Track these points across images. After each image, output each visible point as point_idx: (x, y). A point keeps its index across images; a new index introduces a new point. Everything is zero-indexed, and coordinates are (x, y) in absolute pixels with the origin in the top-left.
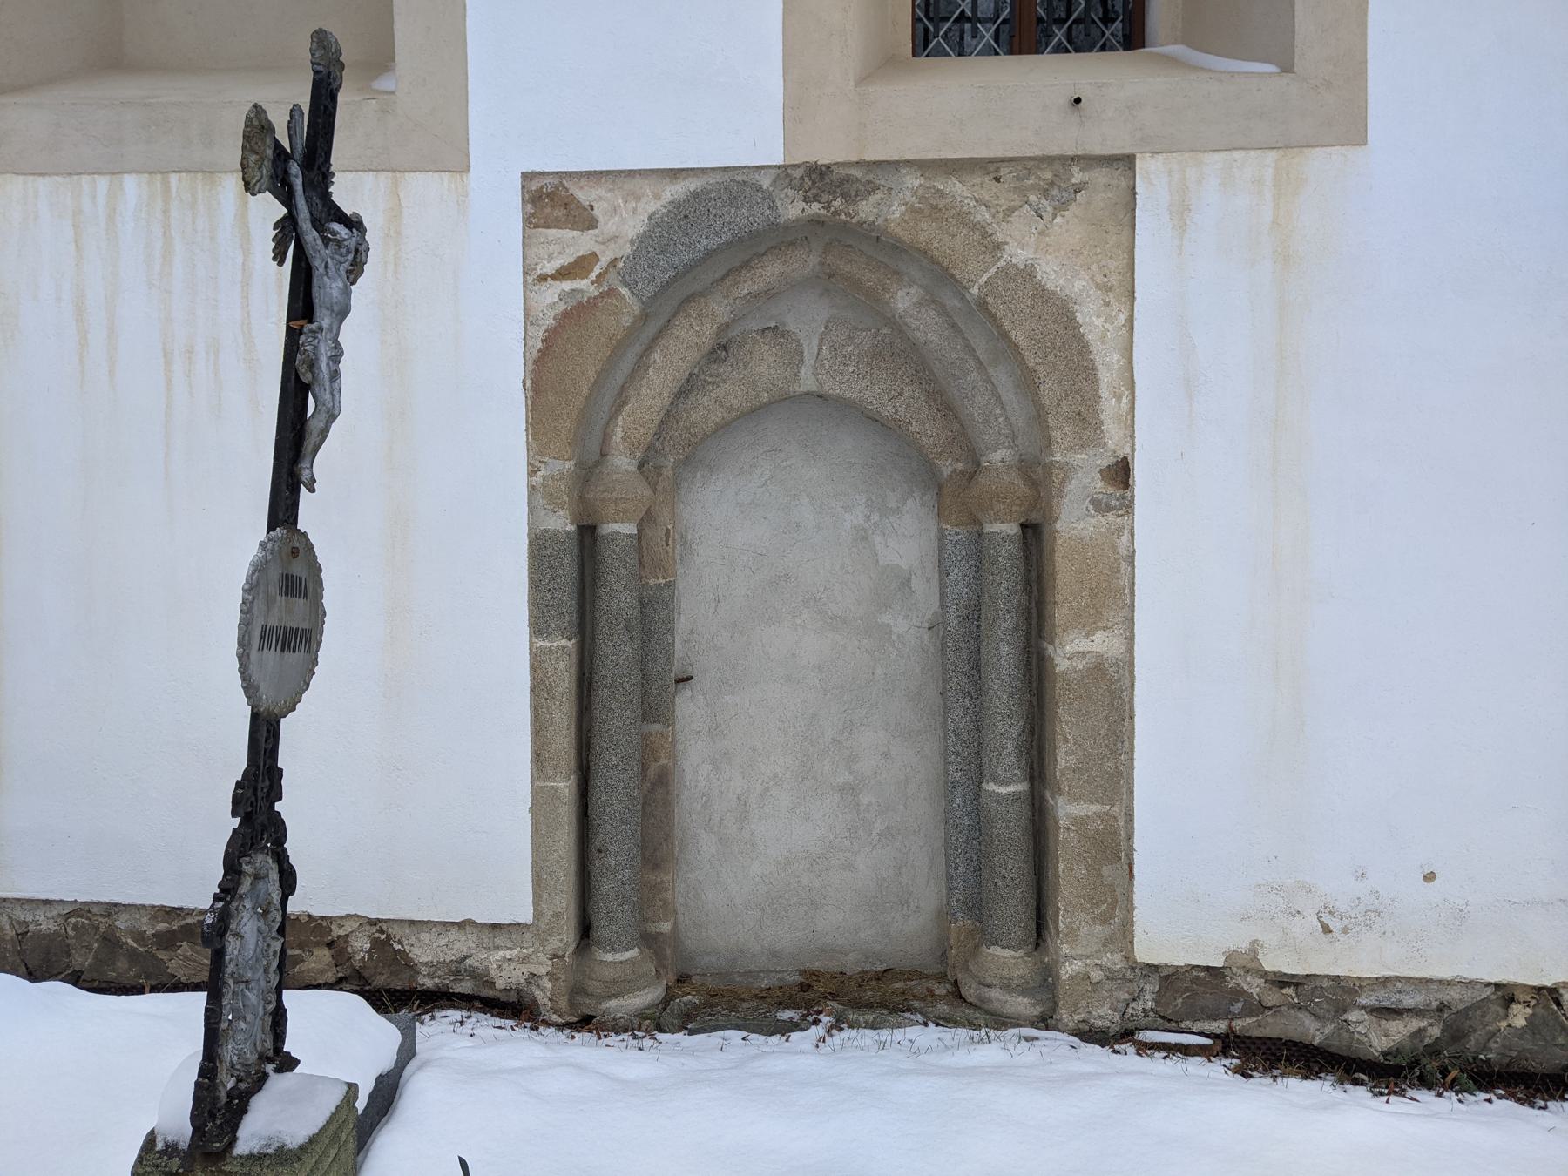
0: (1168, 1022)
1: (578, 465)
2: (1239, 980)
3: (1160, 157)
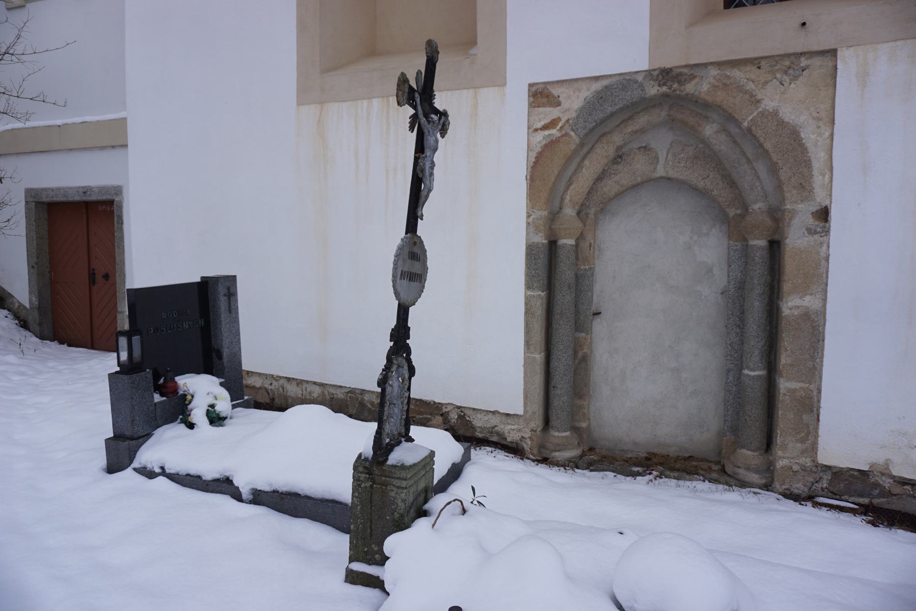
0: (834, 495)
1: (551, 213)
2: (877, 478)
3: (852, 49)
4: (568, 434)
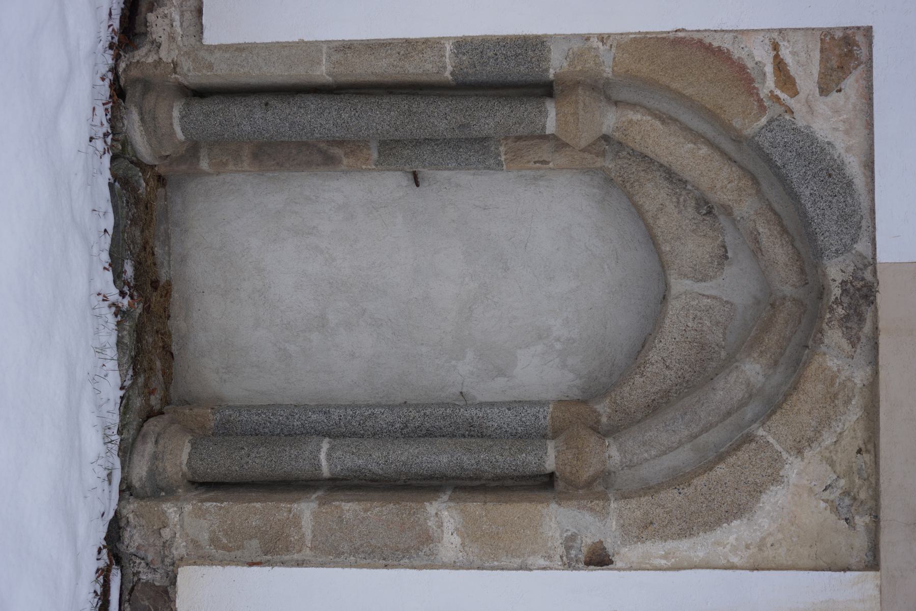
0: (127, 594)
1: (608, 83)
3: (877, 593)
4: (180, 135)
